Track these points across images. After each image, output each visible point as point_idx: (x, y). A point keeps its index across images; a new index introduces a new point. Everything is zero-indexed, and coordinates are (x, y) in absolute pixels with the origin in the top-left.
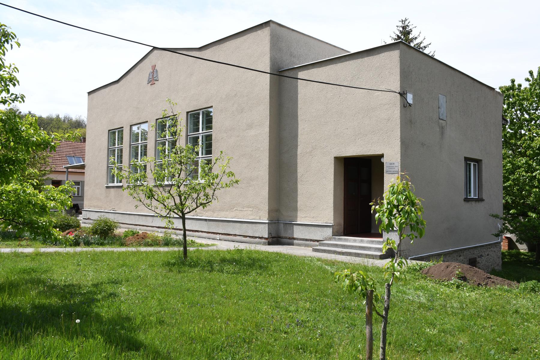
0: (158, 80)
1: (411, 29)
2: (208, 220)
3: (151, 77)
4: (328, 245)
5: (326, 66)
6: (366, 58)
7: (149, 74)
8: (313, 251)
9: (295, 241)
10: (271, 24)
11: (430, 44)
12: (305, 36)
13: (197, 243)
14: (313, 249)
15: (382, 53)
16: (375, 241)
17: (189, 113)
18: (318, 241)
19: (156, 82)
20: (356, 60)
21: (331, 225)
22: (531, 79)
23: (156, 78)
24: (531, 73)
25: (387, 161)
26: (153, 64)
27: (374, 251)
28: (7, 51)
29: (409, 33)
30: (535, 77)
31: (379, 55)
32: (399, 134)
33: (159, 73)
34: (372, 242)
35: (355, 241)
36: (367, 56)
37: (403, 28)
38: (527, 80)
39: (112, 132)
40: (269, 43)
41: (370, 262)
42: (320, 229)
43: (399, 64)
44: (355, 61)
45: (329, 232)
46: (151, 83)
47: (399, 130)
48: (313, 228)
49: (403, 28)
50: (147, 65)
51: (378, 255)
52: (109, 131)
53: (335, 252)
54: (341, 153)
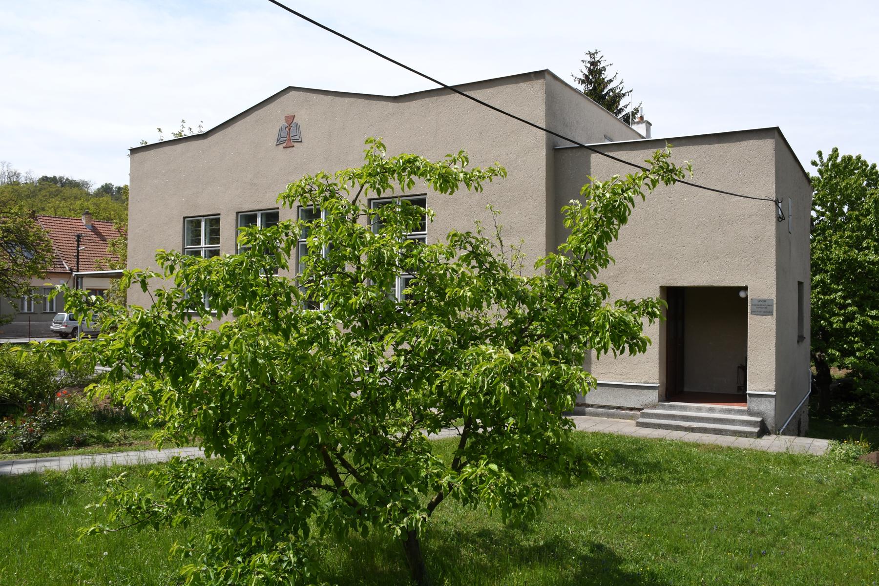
0: (301, 142)
1: (603, 67)
2: (724, 433)
3: (284, 134)
5: (644, 149)
7: (280, 131)
8: (637, 426)
9: (588, 409)
10: (547, 77)
11: (631, 91)
12: (568, 89)
13: (721, 473)
14: (638, 423)
15: (745, 140)
17: (372, 202)
18: (639, 409)
19: (295, 144)
20: (700, 147)
21: (657, 385)
22: (818, 162)
24: (820, 154)
25: (754, 297)
26: (290, 113)
27: (740, 425)
29: (600, 72)
30: (825, 160)
31: (739, 143)
32: (774, 260)
34: (729, 411)
35: (699, 409)
36: (719, 143)
37: (592, 64)
38: (814, 163)
39: (192, 225)
42: (636, 391)
43: (774, 159)
45: (654, 396)
46: (285, 145)
48: (622, 390)
49: (592, 64)
51: (755, 432)
52: (185, 218)
53: (724, 433)
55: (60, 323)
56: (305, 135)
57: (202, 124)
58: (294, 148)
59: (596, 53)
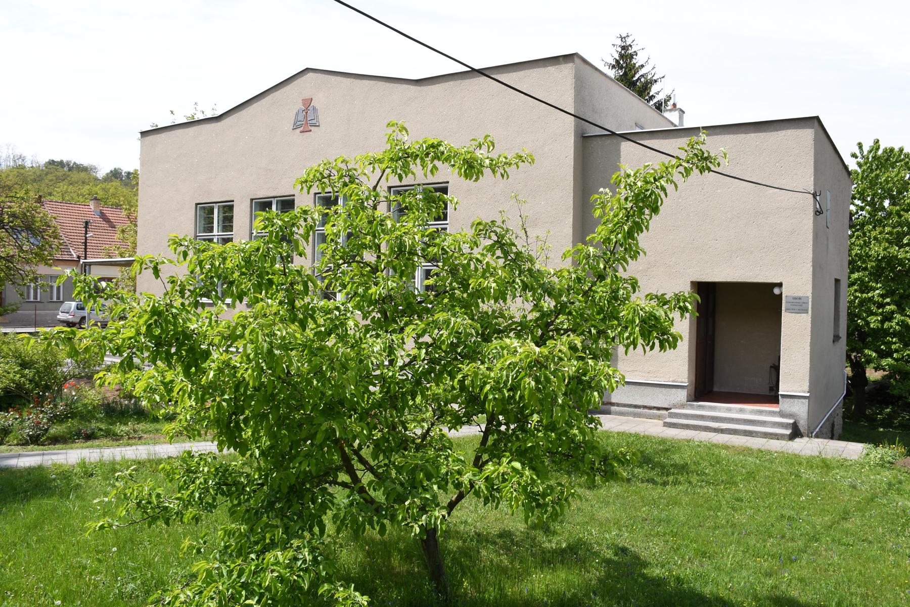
0: (319, 126)
1: (635, 52)
3: (301, 118)
4: (687, 416)
6: (753, 135)
7: (297, 114)
9: (613, 408)
10: (577, 60)
13: (751, 476)
15: (783, 129)
16: (766, 411)
17: (392, 189)
18: (667, 409)
19: (312, 128)
21: (686, 384)
22: (859, 154)
23: (313, 122)
24: (860, 146)
25: (789, 294)
26: (307, 96)
27: (772, 427)
28: (666, 196)
29: (631, 56)
32: (811, 256)
33: (320, 113)
34: (761, 412)
35: (729, 410)
36: (755, 132)
37: (623, 48)
39: (205, 212)
40: (573, 91)
41: (776, 445)
43: (813, 150)
44: (732, 136)
45: (682, 395)
46: (301, 129)
47: (811, 249)
48: (650, 389)
49: (623, 48)
50: (293, 96)
52: (197, 204)
54: (704, 277)
55: (67, 313)
56: (323, 118)
57: (215, 107)
58: (311, 133)
59: (628, 36)
